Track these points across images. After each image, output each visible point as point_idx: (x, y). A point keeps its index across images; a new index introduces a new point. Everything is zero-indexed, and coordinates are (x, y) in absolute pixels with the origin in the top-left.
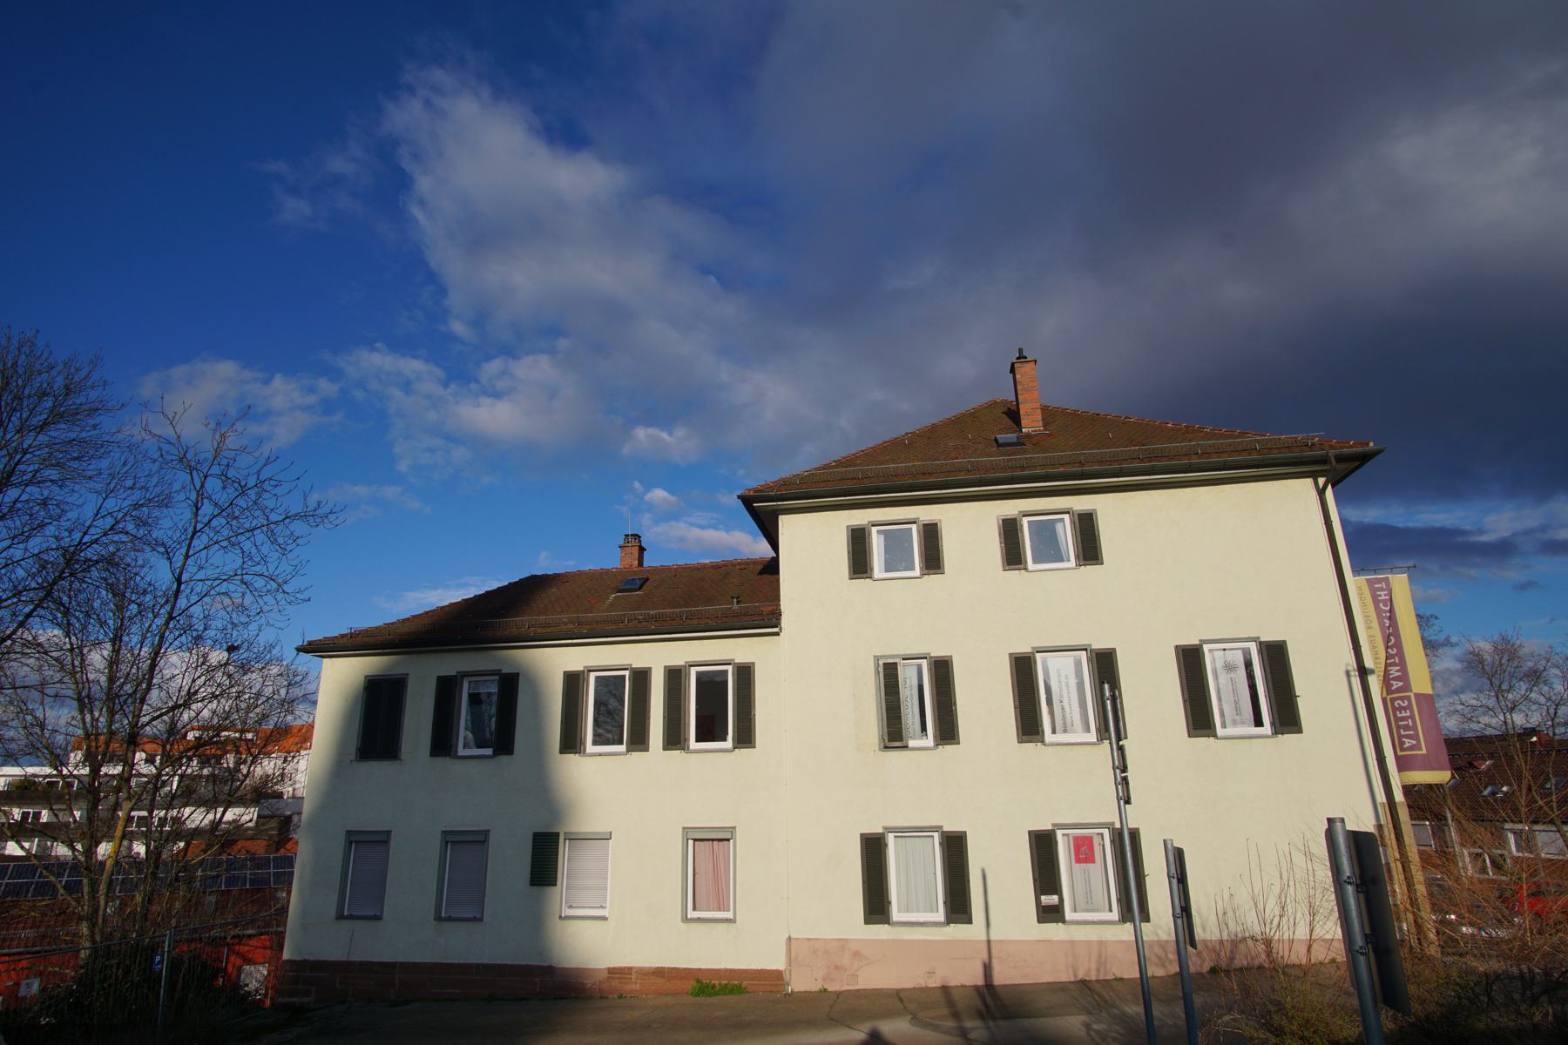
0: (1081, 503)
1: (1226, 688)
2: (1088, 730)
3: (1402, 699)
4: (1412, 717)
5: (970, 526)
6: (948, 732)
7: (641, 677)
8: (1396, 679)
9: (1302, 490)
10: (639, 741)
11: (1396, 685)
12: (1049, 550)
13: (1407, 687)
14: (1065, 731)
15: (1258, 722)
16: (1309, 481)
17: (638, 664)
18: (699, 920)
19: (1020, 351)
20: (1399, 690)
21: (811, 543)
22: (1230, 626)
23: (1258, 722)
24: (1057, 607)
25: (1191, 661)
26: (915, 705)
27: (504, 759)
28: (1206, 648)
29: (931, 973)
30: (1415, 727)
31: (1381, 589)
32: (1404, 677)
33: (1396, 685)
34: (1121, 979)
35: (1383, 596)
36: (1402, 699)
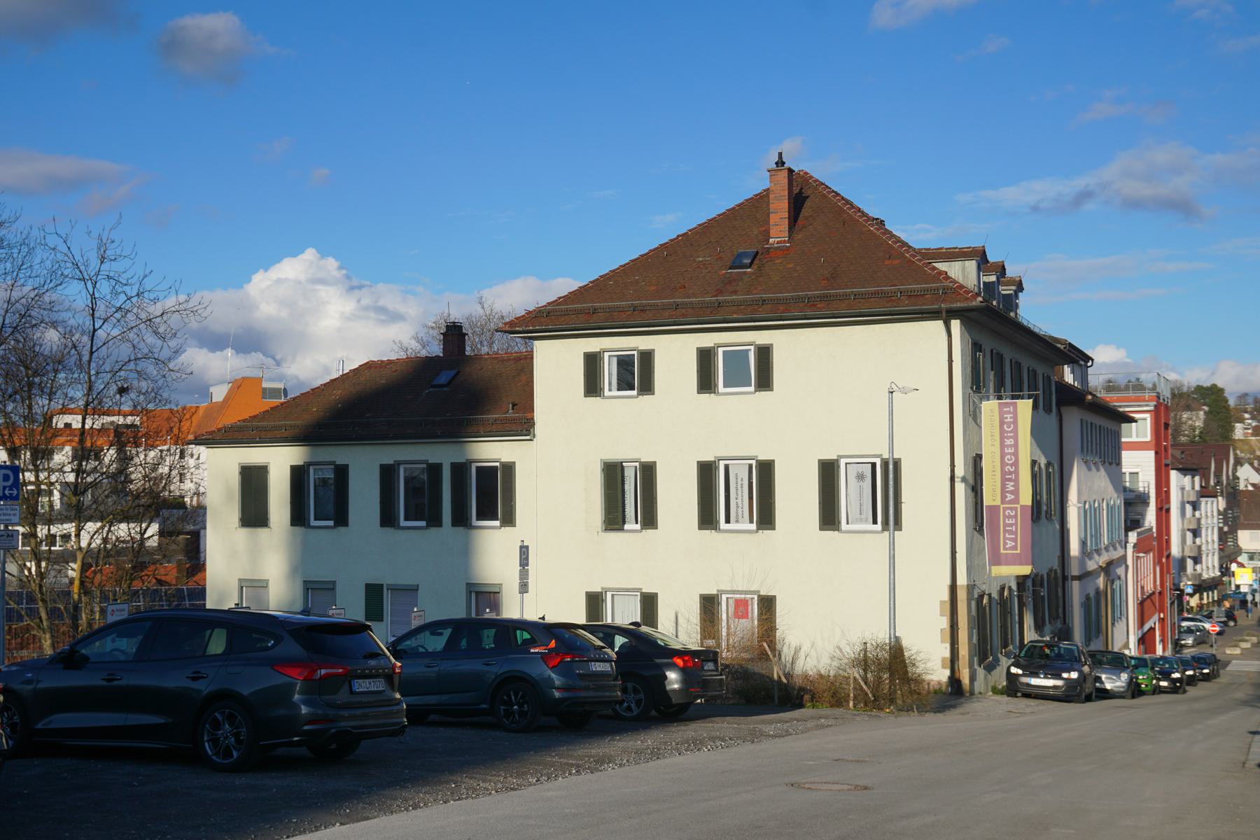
0: (762, 338)
1: (852, 495)
2: (751, 522)
3: (1010, 509)
4: (1016, 524)
5: (675, 354)
6: (649, 520)
7: (435, 470)
8: (1011, 492)
9: (935, 328)
10: (435, 520)
11: (1010, 497)
12: (736, 378)
13: (1016, 501)
14: (737, 521)
15: (875, 522)
16: (939, 324)
17: (433, 460)
18: (408, 528)
19: (780, 154)
20: (1010, 502)
21: (556, 364)
22: (858, 443)
23: (875, 522)
24: (736, 426)
25: (828, 471)
26: (626, 495)
27: (342, 529)
28: (843, 462)
29: (543, 618)
30: (1005, 531)
31: (1009, 412)
32: (1016, 492)
33: (1010, 497)
34: (255, 416)
35: (1009, 418)
36: (1010, 509)
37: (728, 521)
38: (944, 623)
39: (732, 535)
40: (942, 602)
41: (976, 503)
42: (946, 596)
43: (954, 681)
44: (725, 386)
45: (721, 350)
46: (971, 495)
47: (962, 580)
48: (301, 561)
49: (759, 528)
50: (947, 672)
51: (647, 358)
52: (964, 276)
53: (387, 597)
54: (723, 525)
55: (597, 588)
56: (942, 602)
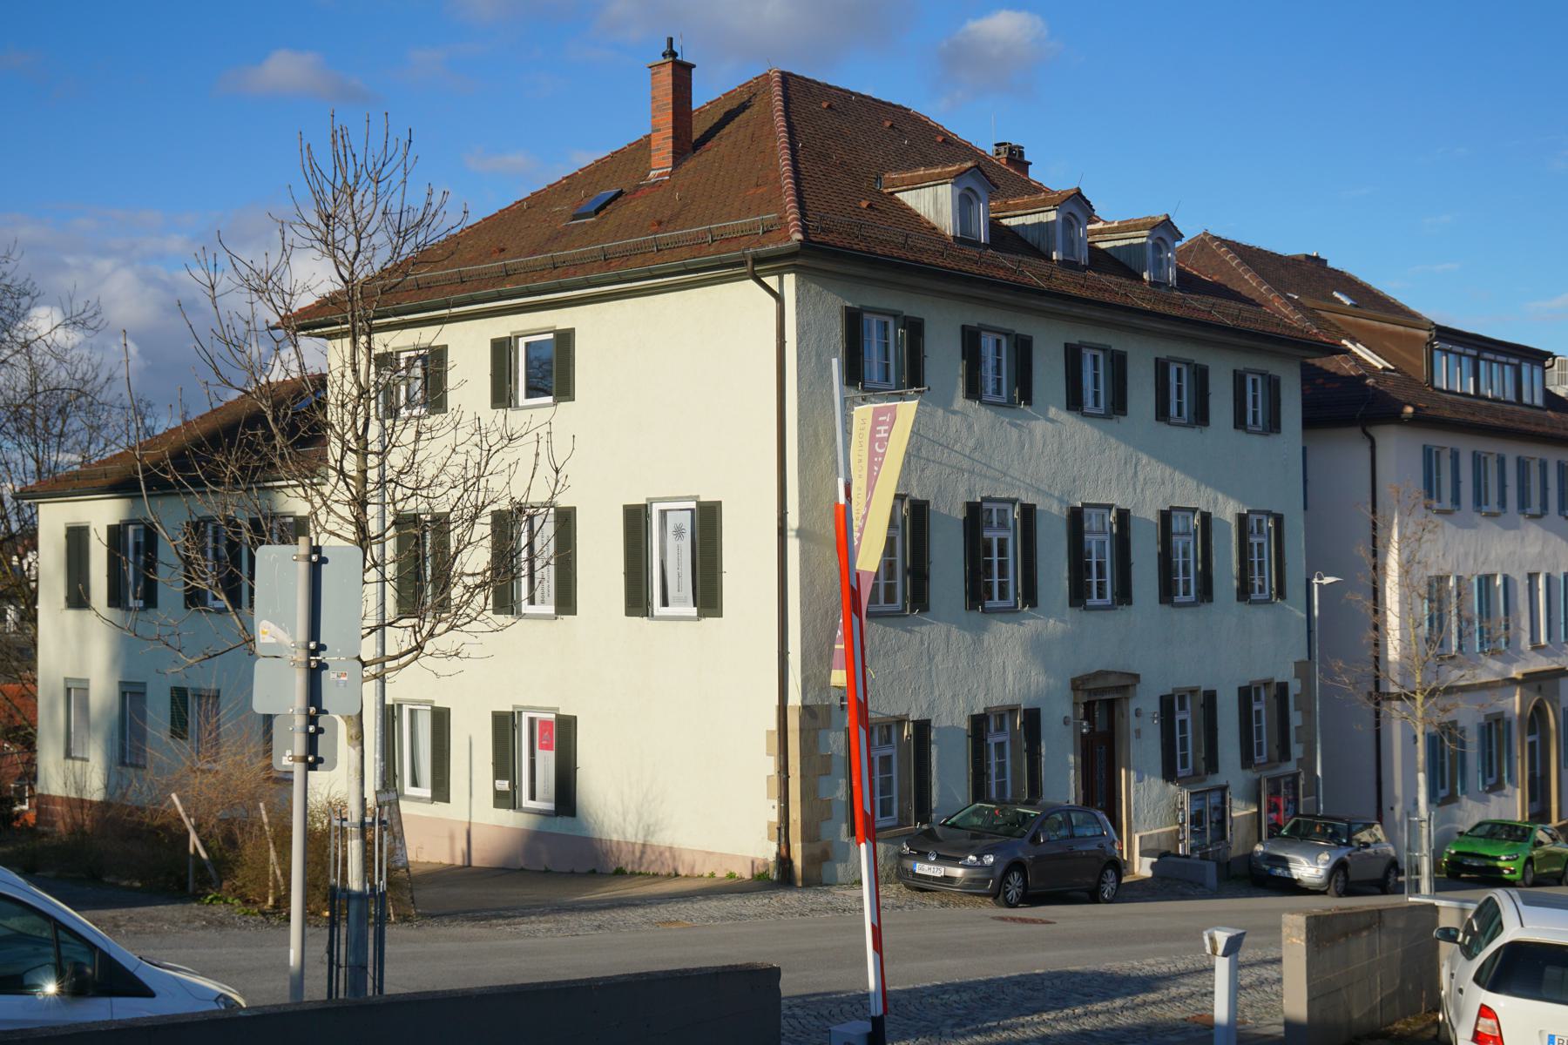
14: (543, 602)
22: (671, 486)
28: (656, 509)
37: (665, 603)
38: (770, 766)
39: (674, 623)
40: (769, 733)
41: (1488, 605)
42: (773, 724)
43: (784, 861)
44: (528, 396)
45: (522, 342)
46: (1379, 584)
47: (795, 699)
48: (128, 647)
49: (558, 612)
50: (774, 847)
51: (565, 339)
52: (937, 212)
53: (193, 704)
54: (526, 608)
55: (507, 708)
56: (769, 733)
